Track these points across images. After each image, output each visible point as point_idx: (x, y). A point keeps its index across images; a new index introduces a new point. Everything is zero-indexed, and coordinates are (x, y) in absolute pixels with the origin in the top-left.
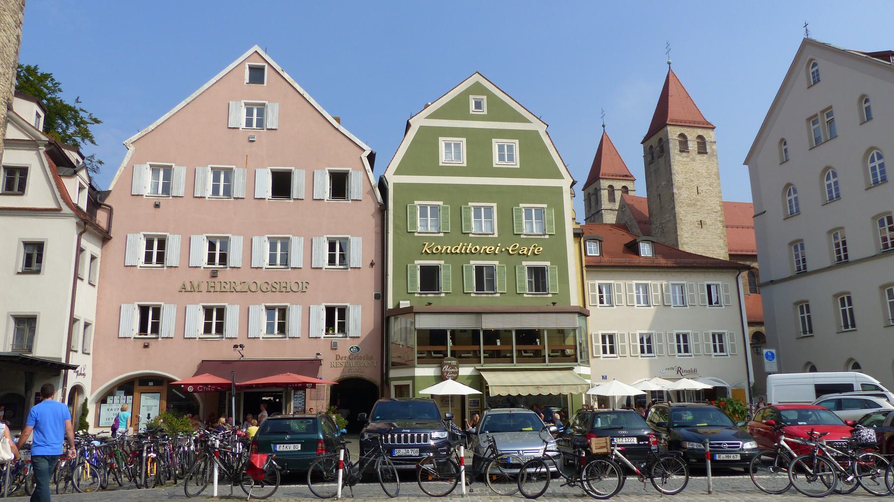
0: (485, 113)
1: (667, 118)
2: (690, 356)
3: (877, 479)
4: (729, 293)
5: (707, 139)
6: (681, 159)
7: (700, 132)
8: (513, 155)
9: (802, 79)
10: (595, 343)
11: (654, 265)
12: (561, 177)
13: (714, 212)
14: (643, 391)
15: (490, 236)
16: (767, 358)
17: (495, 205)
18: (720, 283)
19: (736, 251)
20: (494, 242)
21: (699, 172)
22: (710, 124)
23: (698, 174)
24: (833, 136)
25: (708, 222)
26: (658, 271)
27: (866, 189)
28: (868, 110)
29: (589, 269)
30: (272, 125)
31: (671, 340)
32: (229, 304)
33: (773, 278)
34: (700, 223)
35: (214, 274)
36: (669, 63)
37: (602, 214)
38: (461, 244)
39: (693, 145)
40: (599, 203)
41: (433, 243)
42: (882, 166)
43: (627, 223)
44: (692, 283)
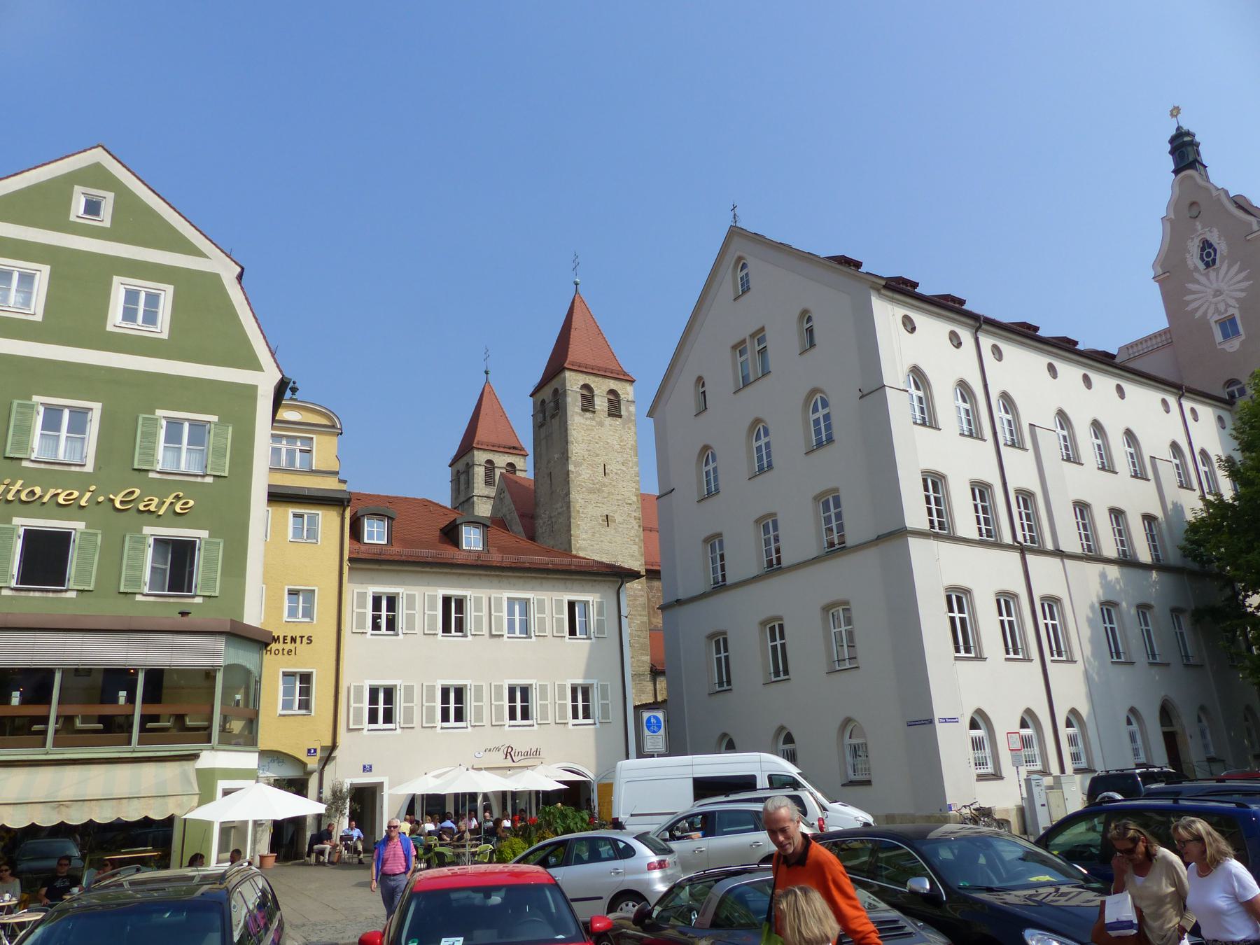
0: (107, 223)
1: (566, 360)
2: (530, 726)
3: (1217, 458)
5: (622, 396)
6: (582, 421)
7: (613, 385)
8: (156, 313)
9: (727, 287)
10: (355, 703)
11: (480, 563)
13: (627, 504)
14: (560, 782)
15: (73, 469)
16: (648, 728)
17: (97, 407)
19: (652, 565)
20: (82, 481)
21: (608, 443)
23: (607, 446)
24: (765, 373)
25: (618, 518)
26: (486, 575)
27: (806, 454)
28: (810, 331)
29: (355, 566)
33: (681, 597)
34: (605, 518)
36: (576, 284)
37: (473, 503)
39: (601, 403)
42: (827, 417)
43: (505, 516)
44: (543, 598)
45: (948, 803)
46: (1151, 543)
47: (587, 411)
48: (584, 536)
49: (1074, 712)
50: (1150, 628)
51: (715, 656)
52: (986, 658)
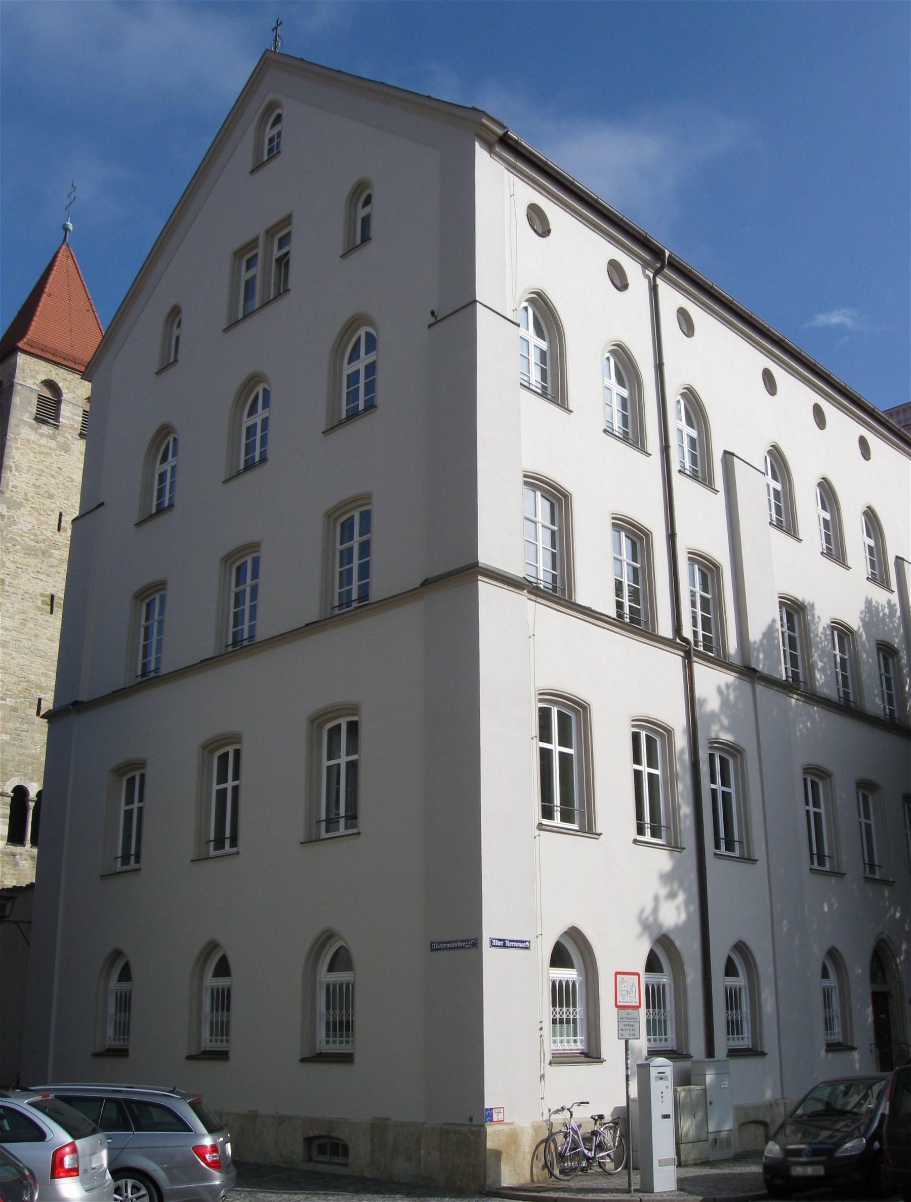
6: (33, 436)
42: (371, 369)
45: (487, 1106)
46: (885, 691)
47: (44, 422)
49: (741, 948)
50: (872, 822)
51: (123, 808)
52: (599, 835)
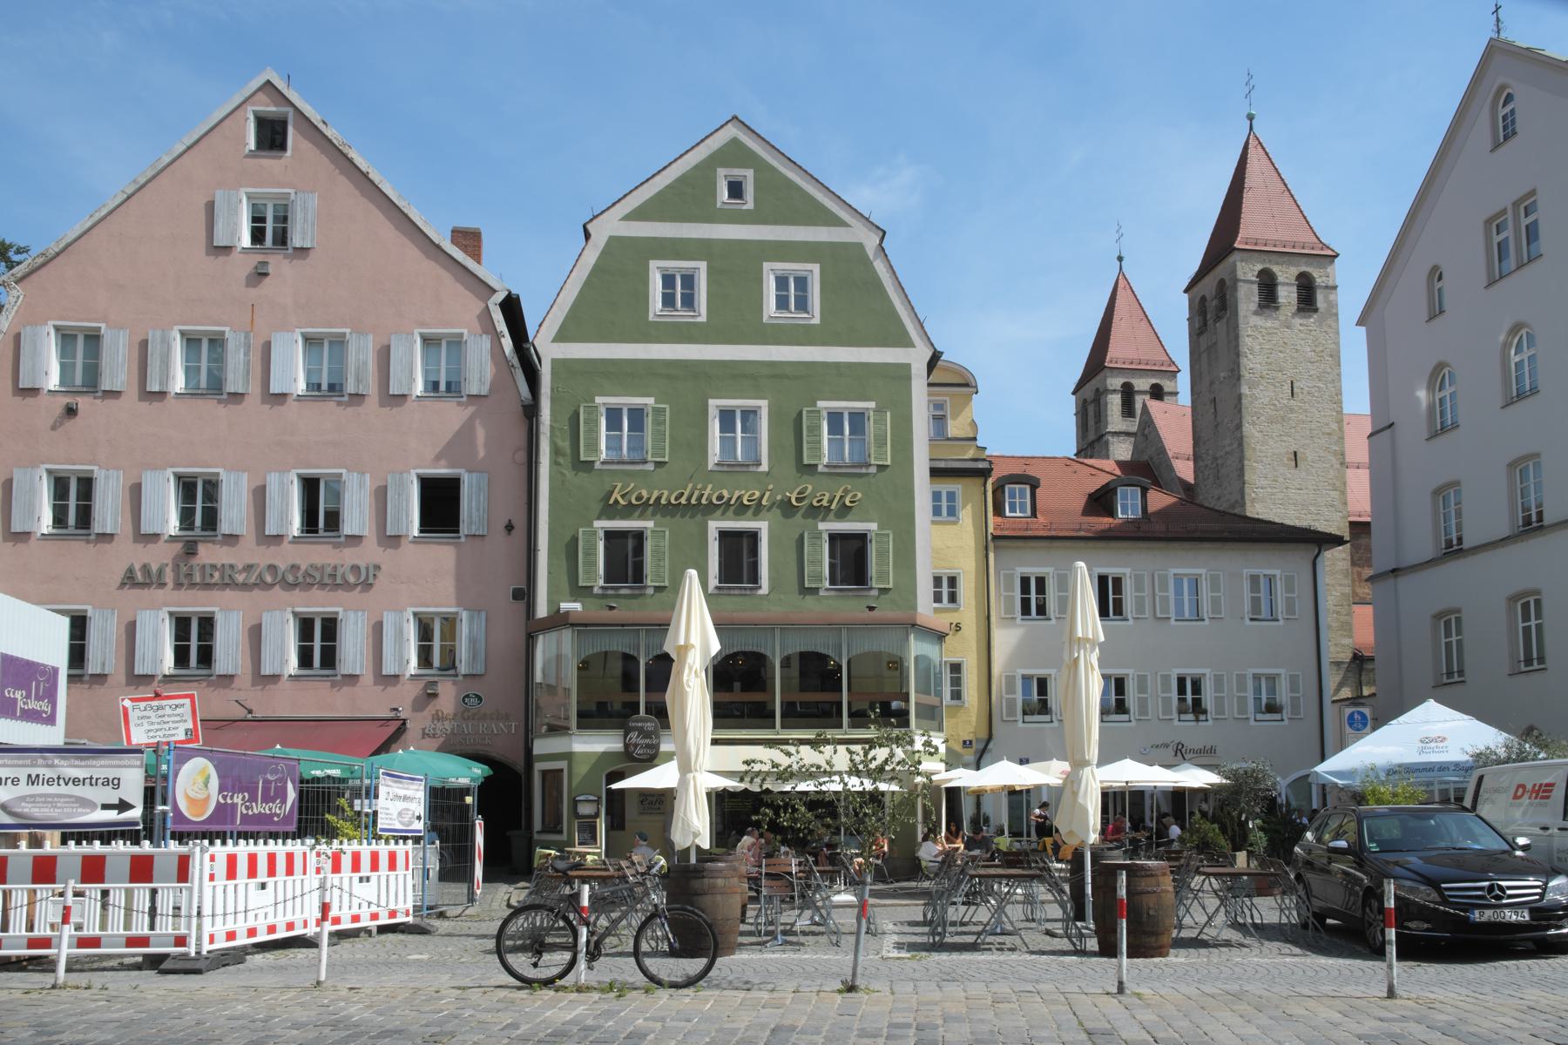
1: (1237, 236)
4: (1294, 593)
5: (1318, 281)
9: (1481, 131)
12: (910, 344)
13: (1323, 434)
16: (1351, 725)
17: (763, 404)
18: (1277, 572)
22: (1328, 247)
30: (303, 239)
31: (1166, 688)
32: (221, 610)
35: (190, 550)
37: (1107, 443)
38: (690, 486)
40: (1102, 418)
41: (632, 485)
43: (1151, 458)
48: (1264, 482)
51: (1444, 640)
